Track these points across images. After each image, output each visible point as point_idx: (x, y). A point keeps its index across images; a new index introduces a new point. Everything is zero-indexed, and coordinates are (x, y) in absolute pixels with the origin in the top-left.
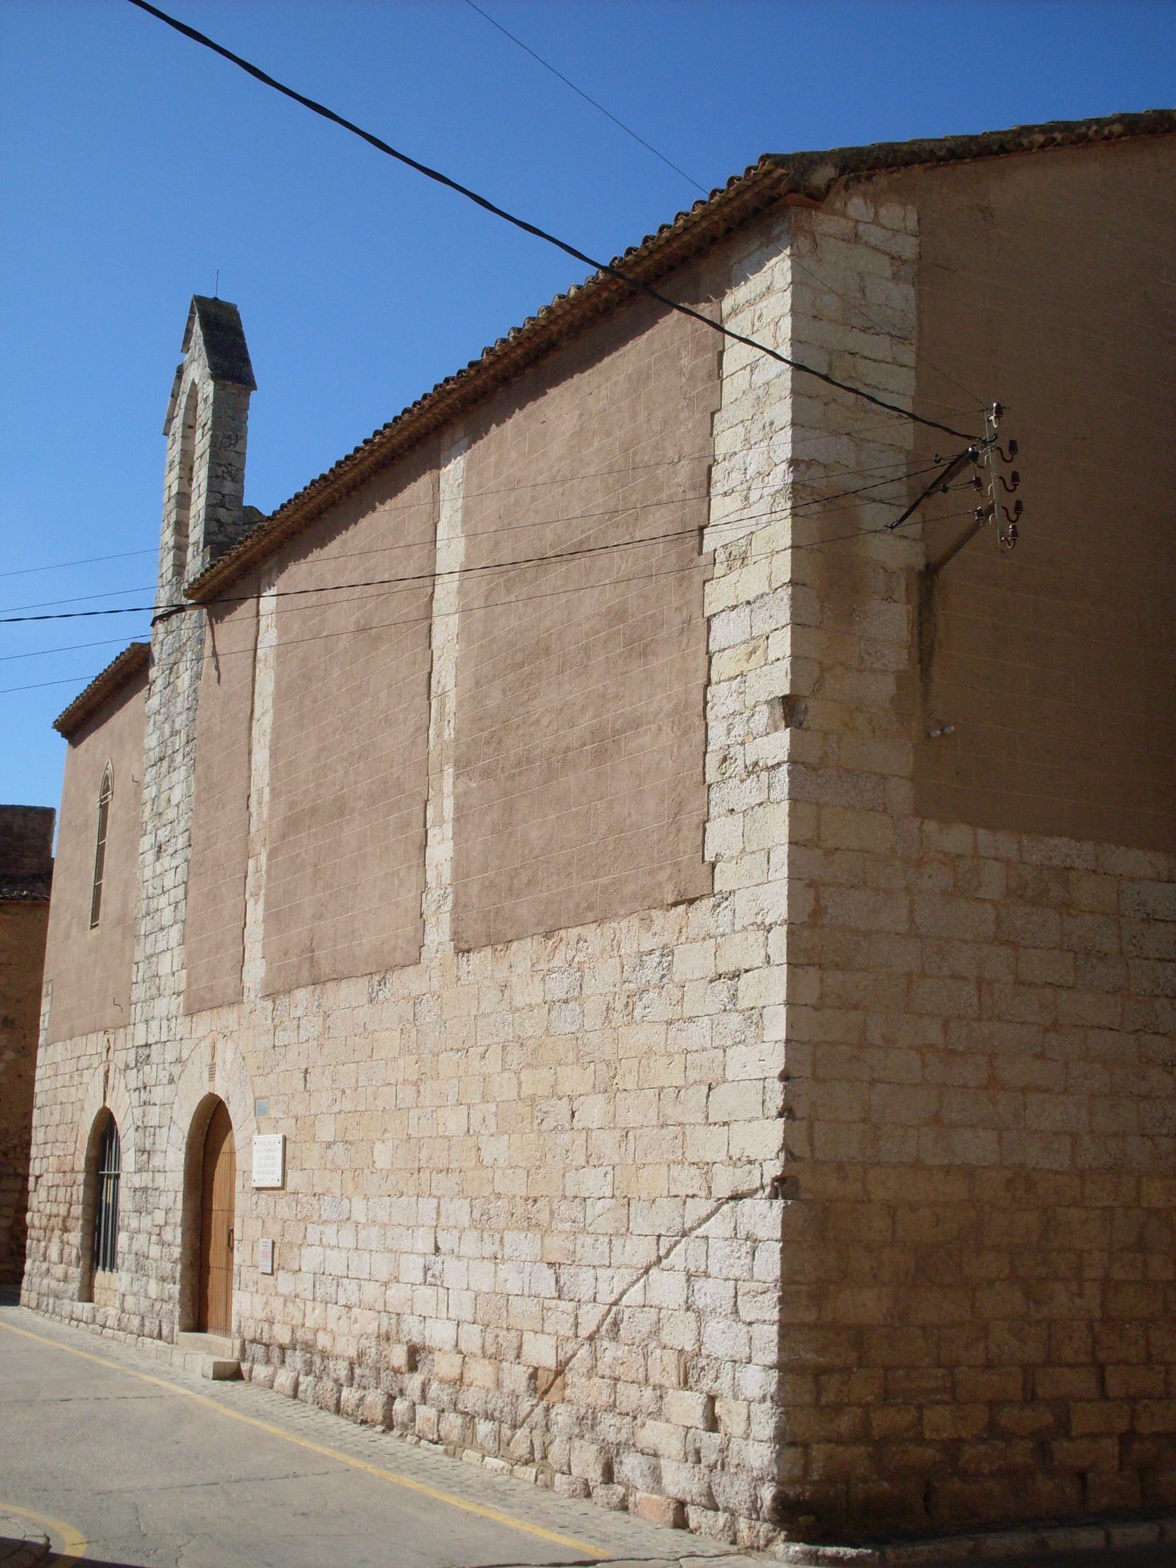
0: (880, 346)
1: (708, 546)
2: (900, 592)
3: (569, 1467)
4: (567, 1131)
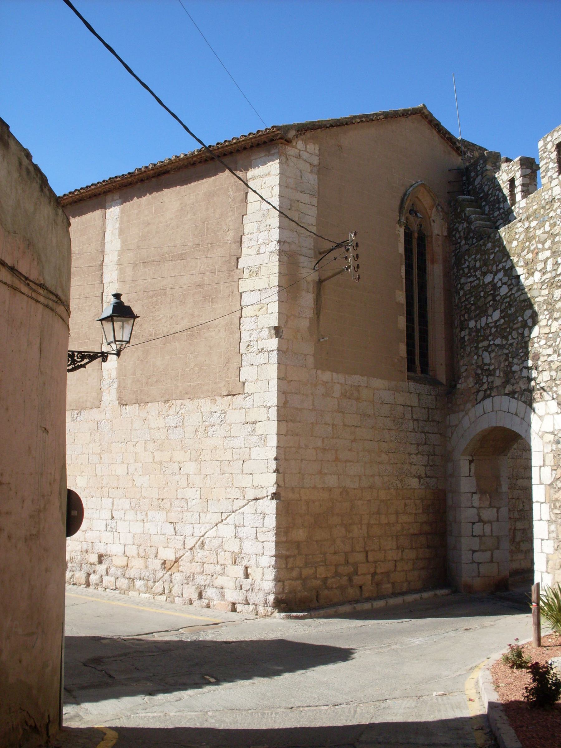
0: (305, 198)
1: (241, 265)
2: (311, 290)
3: (182, 594)
4: (177, 475)
